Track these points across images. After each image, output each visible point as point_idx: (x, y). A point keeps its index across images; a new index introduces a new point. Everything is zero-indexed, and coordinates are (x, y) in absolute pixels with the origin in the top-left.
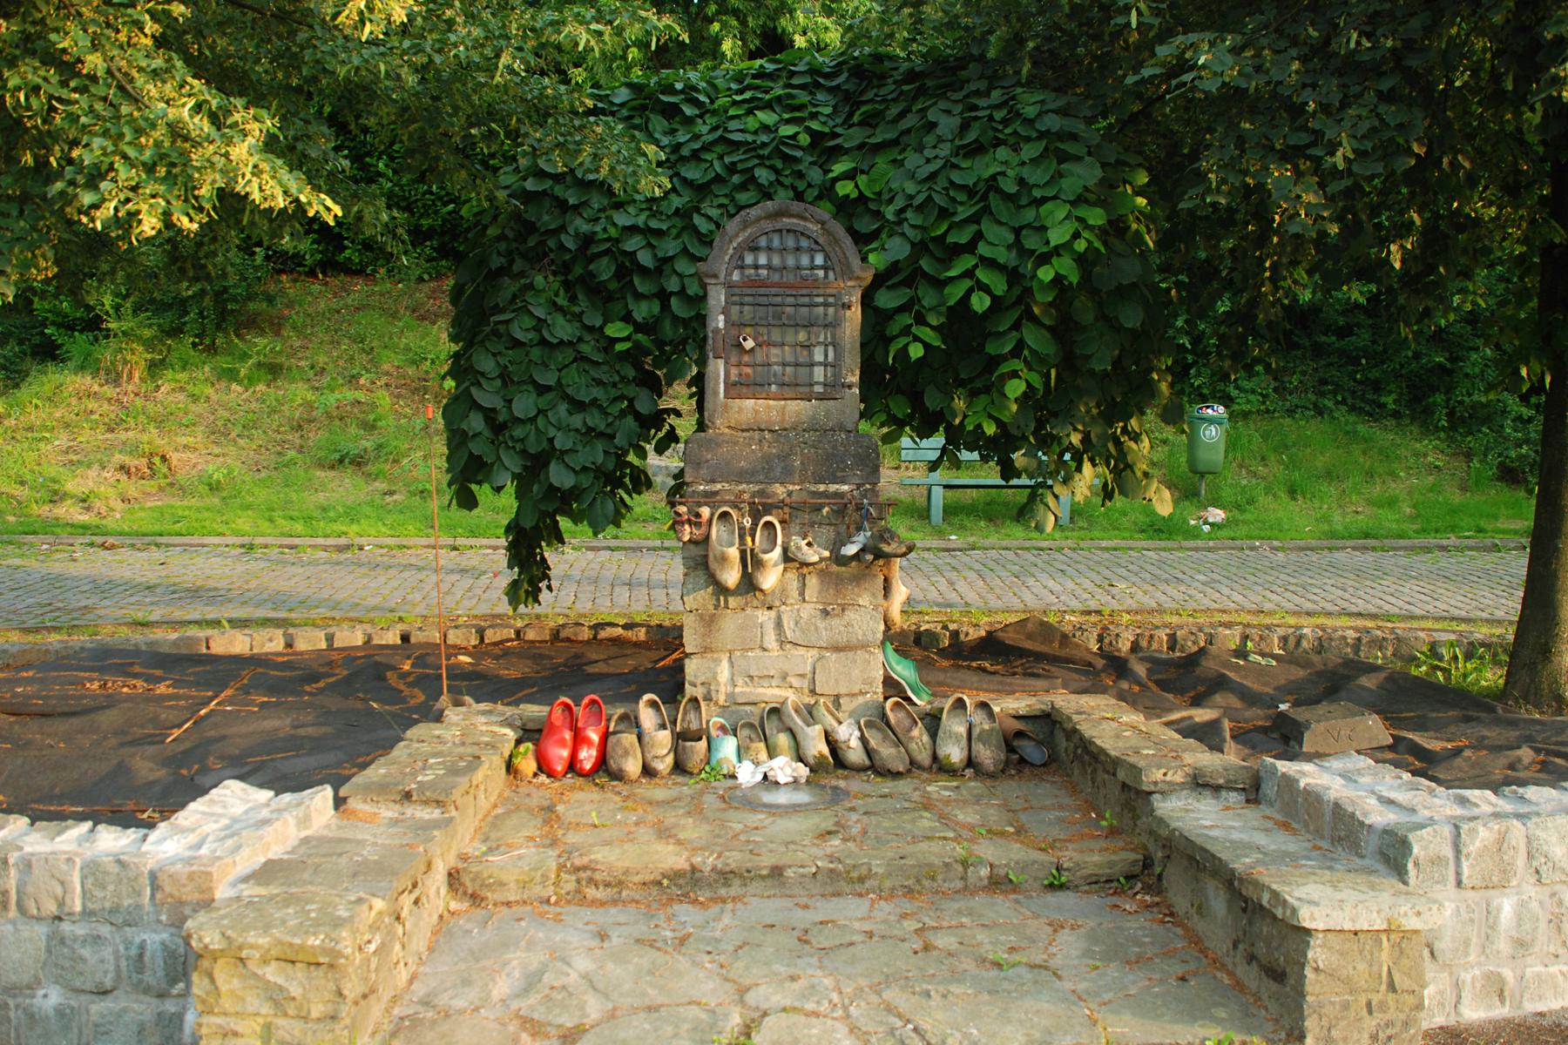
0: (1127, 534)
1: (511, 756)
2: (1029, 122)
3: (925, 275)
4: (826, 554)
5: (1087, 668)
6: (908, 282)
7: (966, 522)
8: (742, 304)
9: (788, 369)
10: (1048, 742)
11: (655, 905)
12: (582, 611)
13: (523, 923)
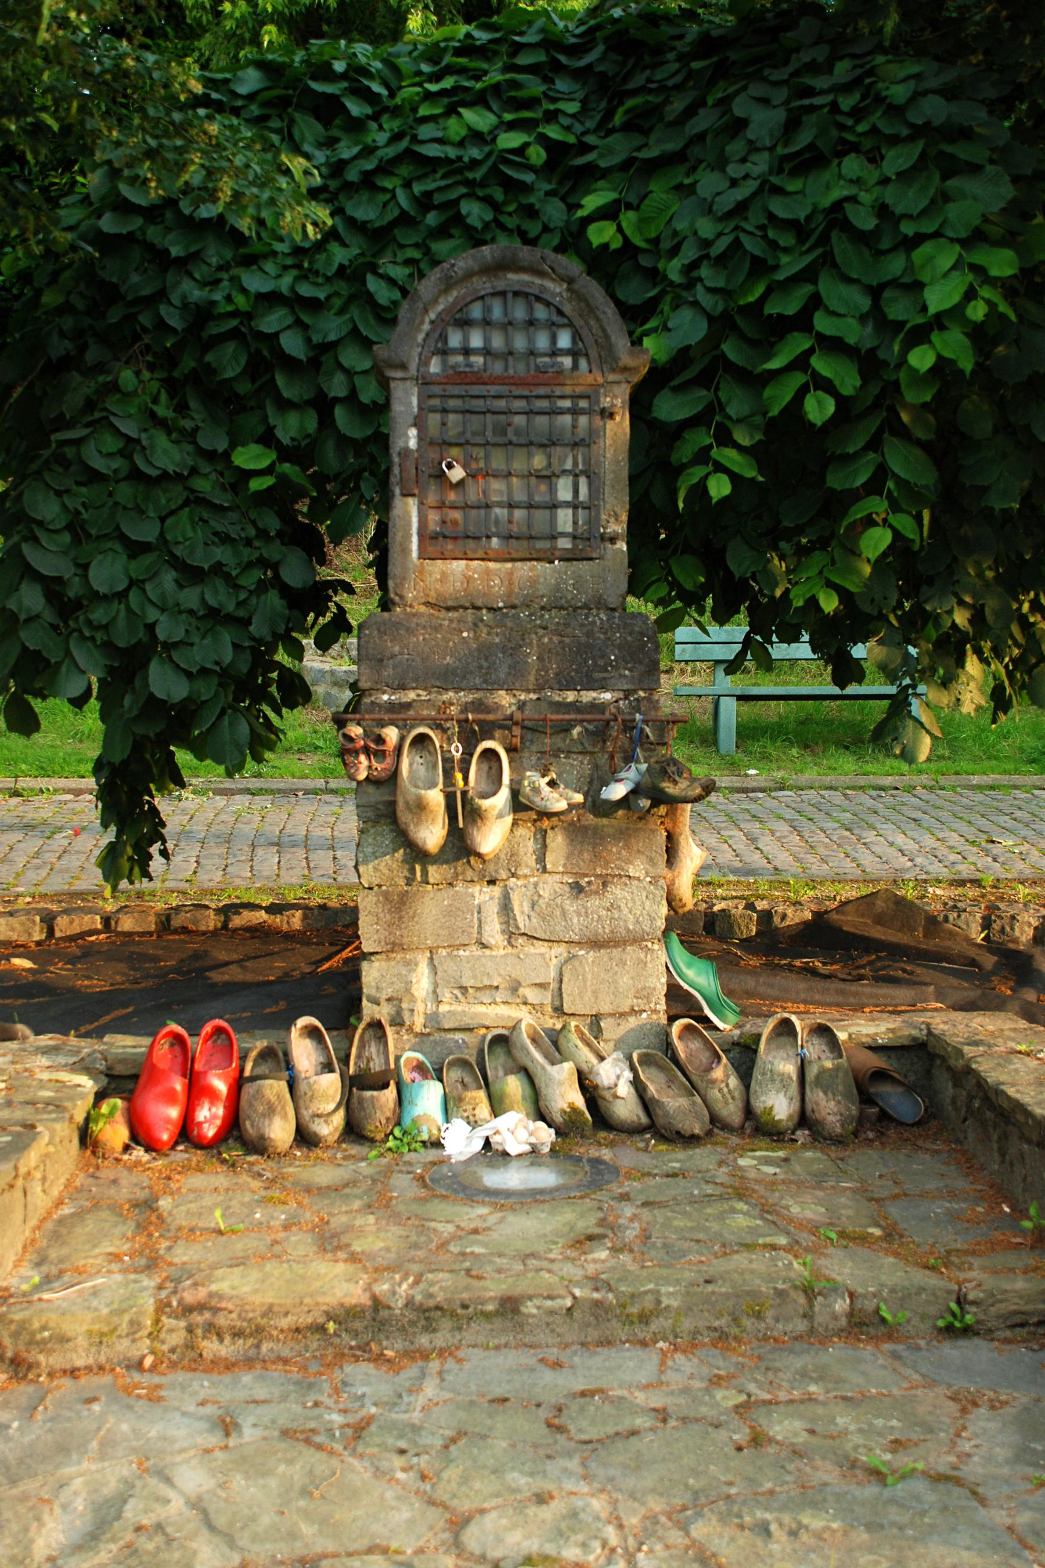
0: (1010, 766)
1: (87, 1119)
2: (896, 111)
3: (729, 366)
4: (579, 798)
5: (967, 967)
6: (705, 379)
7: (770, 749)
8: (445, 411)
9: (519, 514)
10: (923, 1086)
11: (314, 1367)
12: (207, 885)
13: (96, 1407)
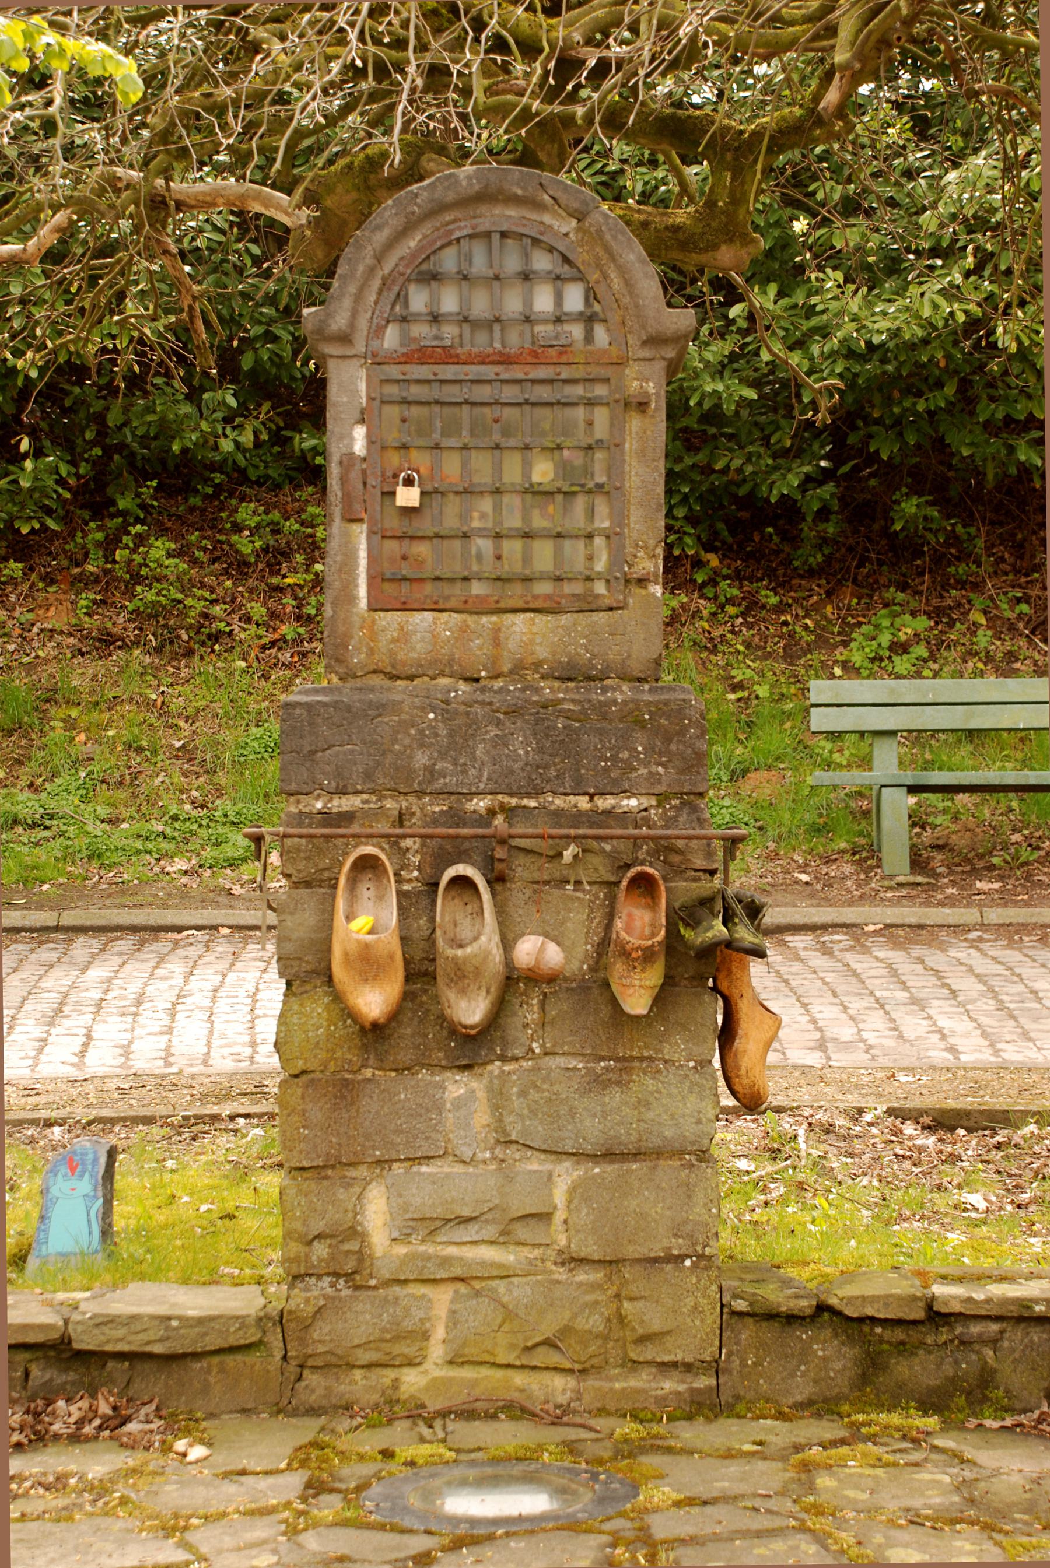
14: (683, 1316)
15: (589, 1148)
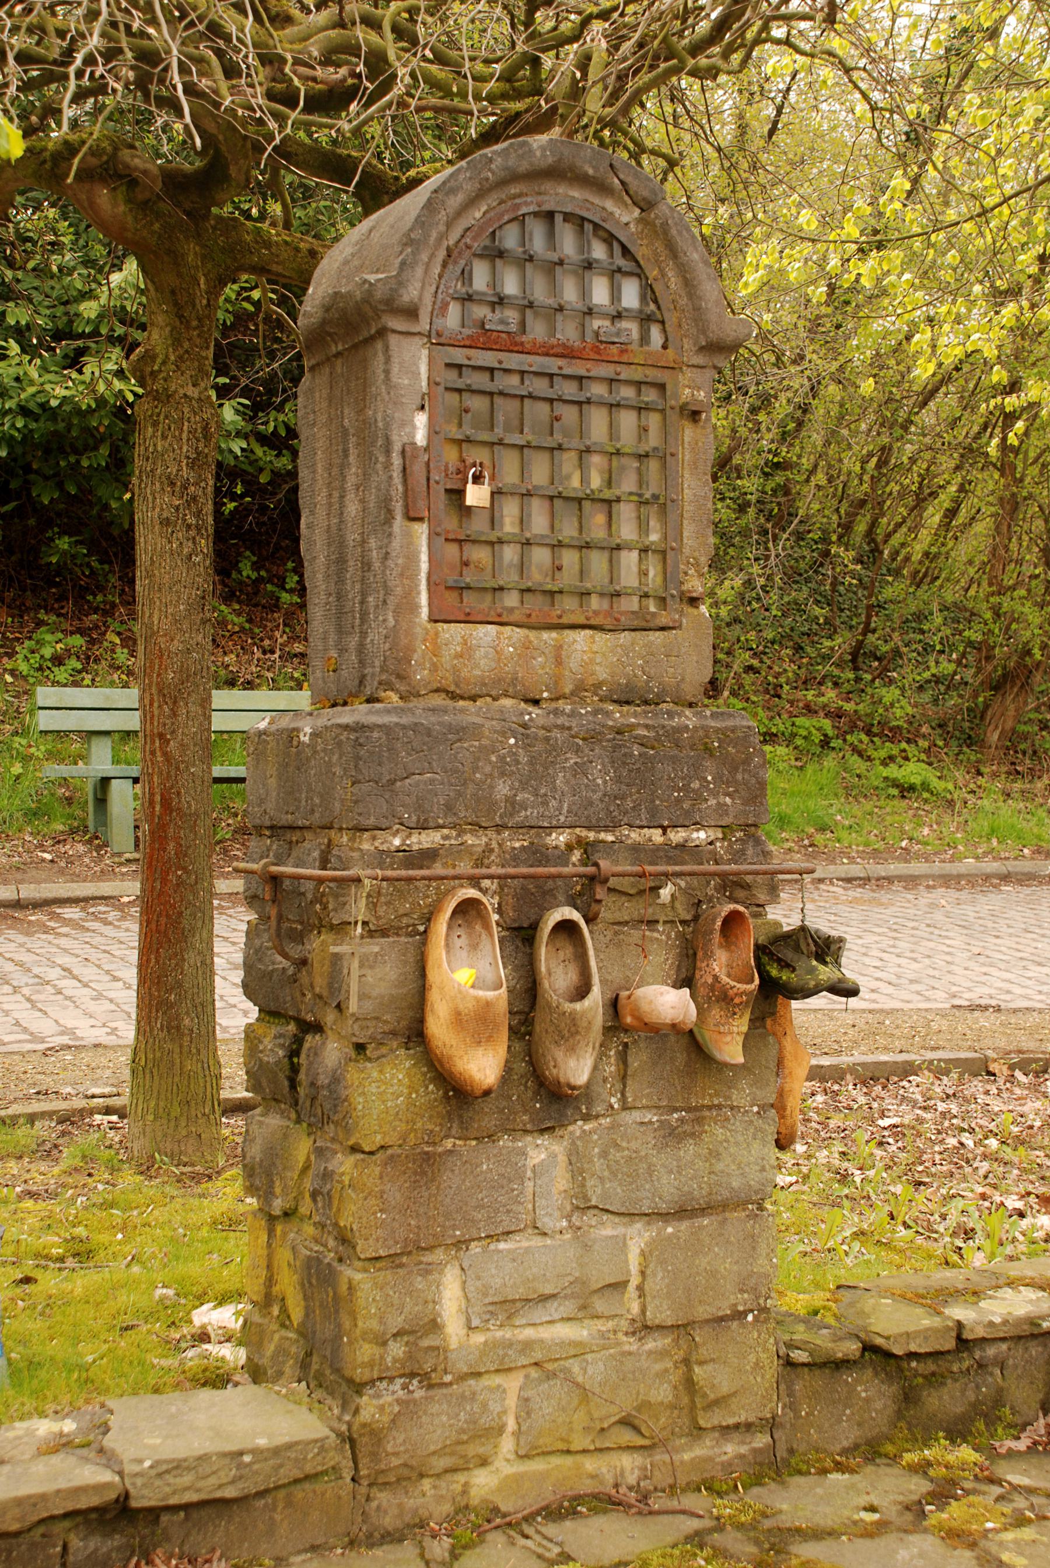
8: (614, 406)
14: (742, 1374)
15: (663, 1207)
